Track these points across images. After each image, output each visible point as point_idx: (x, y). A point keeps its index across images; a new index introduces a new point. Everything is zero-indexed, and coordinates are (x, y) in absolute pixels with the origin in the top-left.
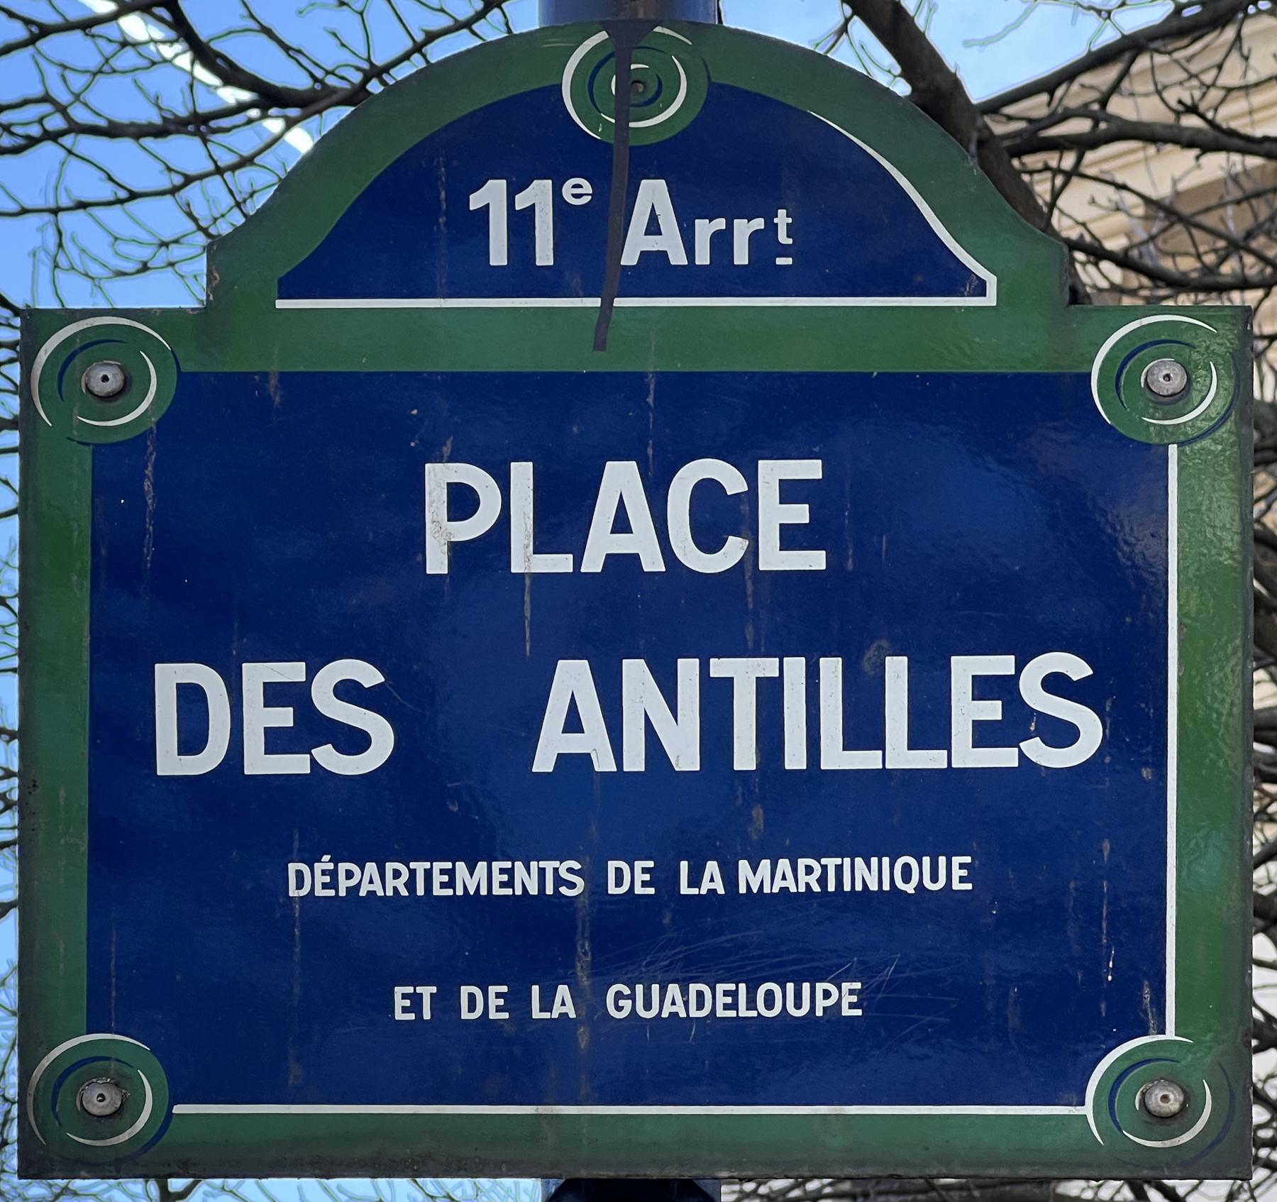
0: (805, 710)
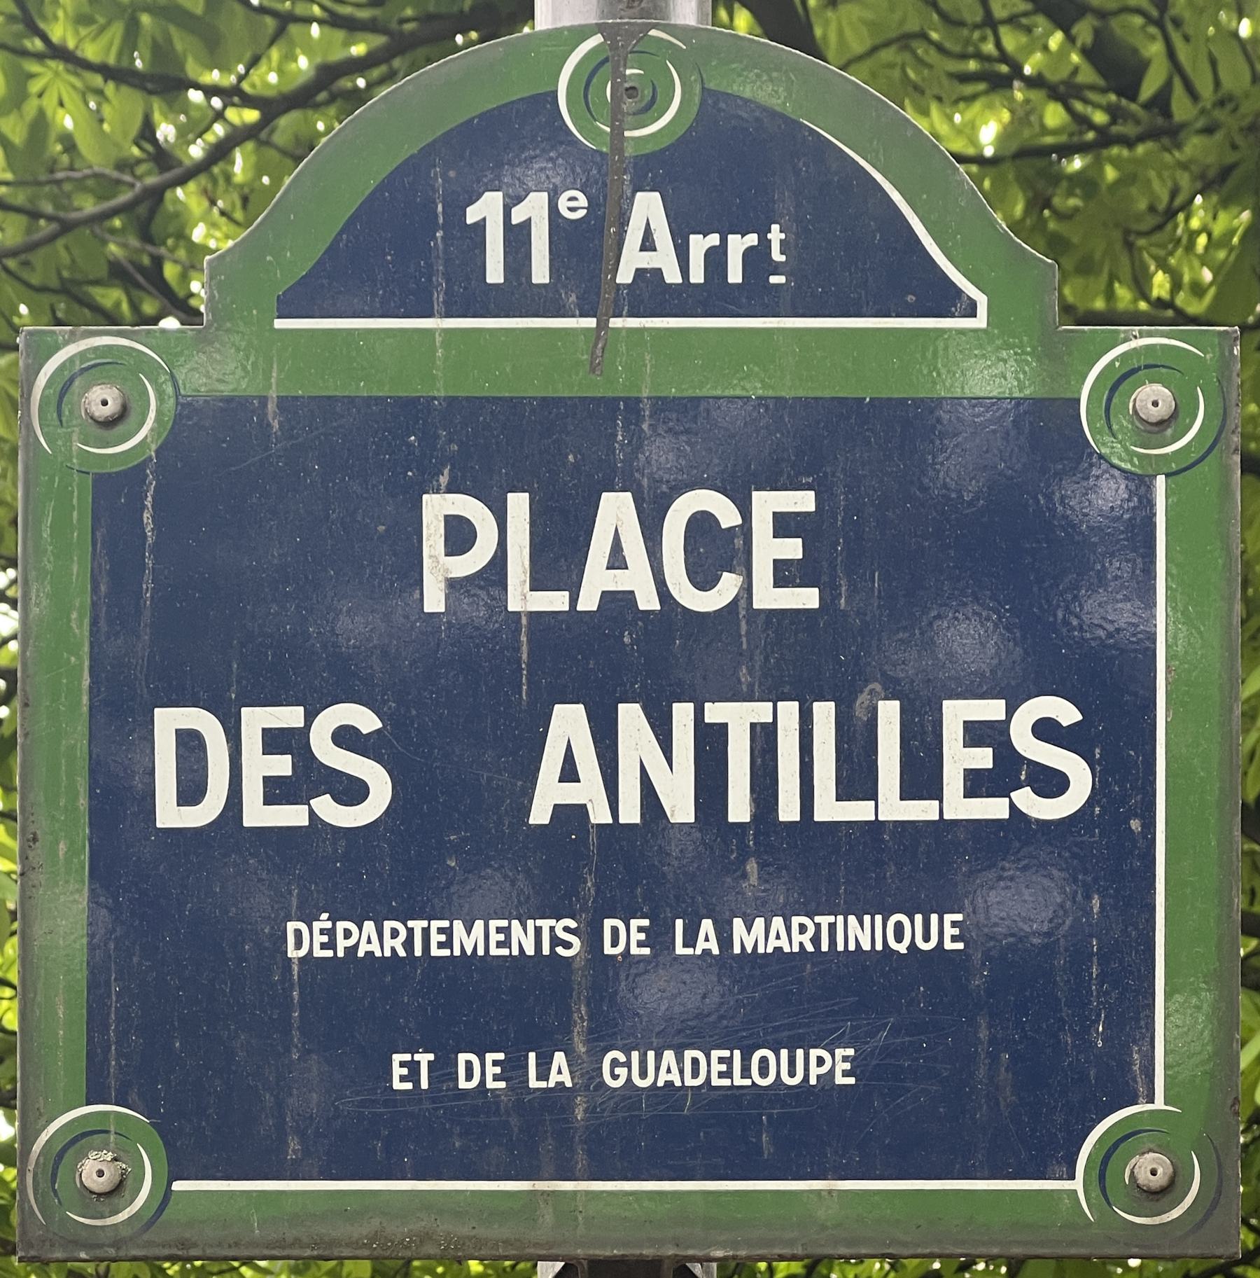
0: (793, 758)
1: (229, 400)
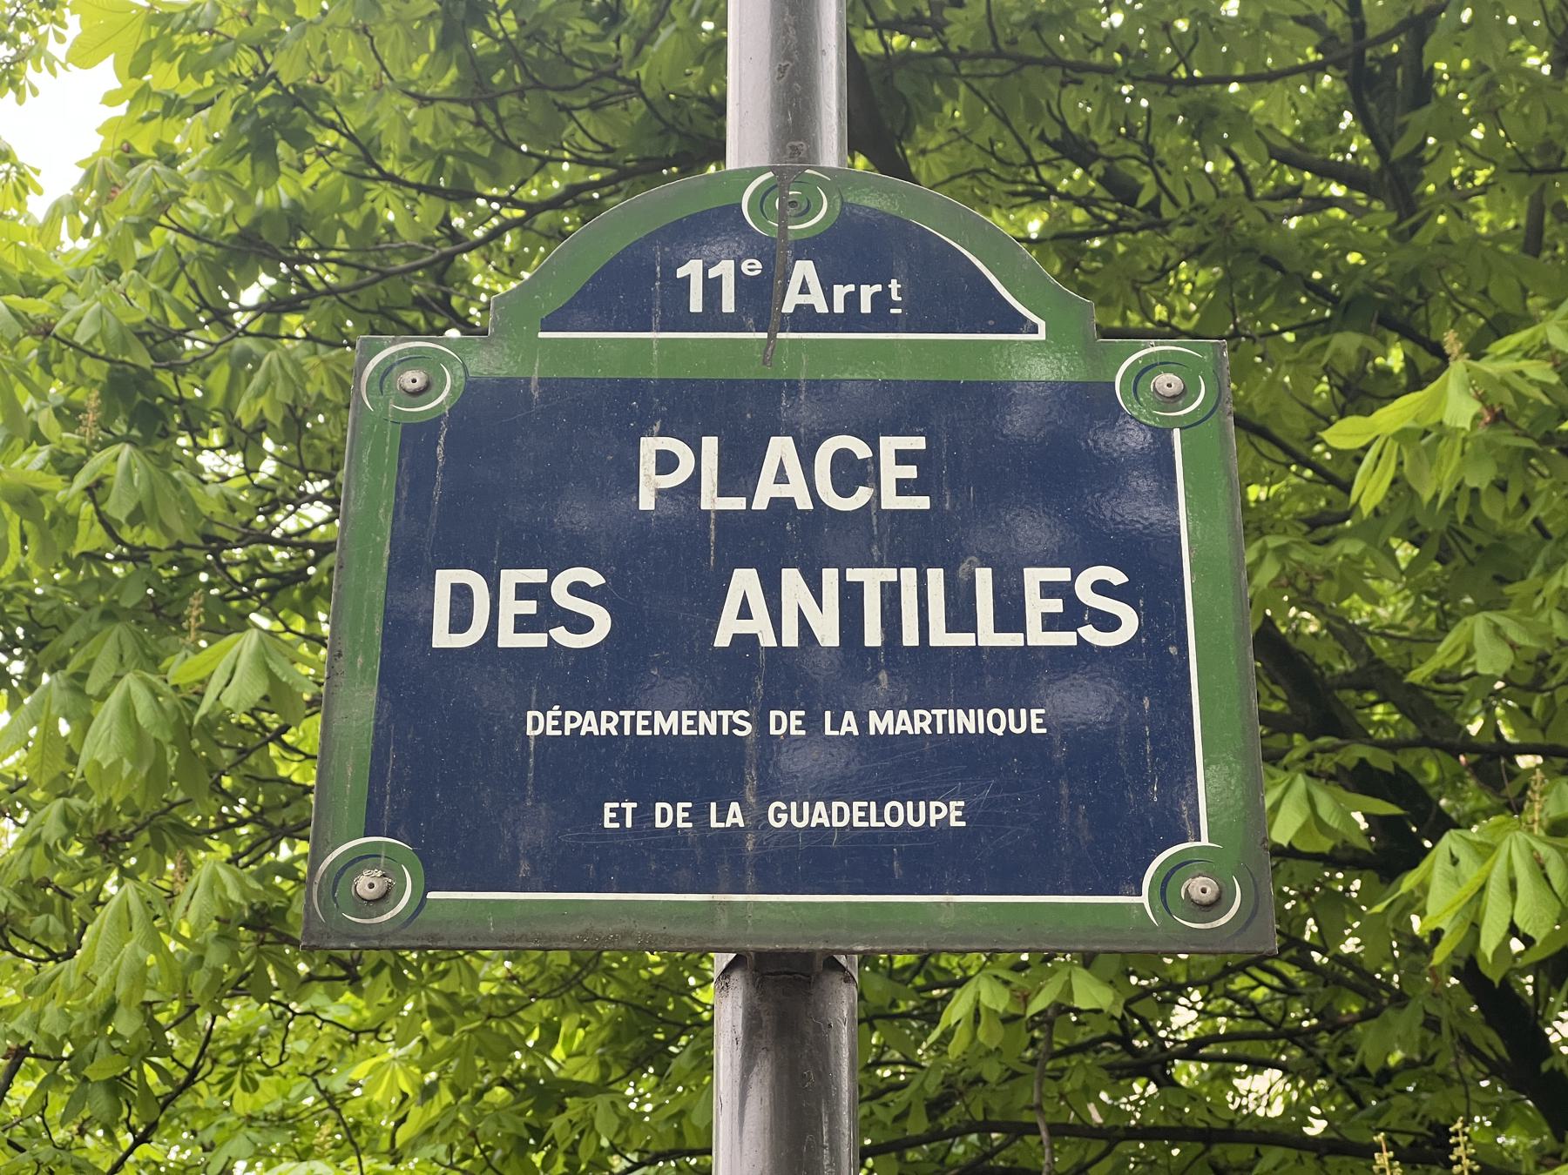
0: (920, 606)
1: (503, 380)
